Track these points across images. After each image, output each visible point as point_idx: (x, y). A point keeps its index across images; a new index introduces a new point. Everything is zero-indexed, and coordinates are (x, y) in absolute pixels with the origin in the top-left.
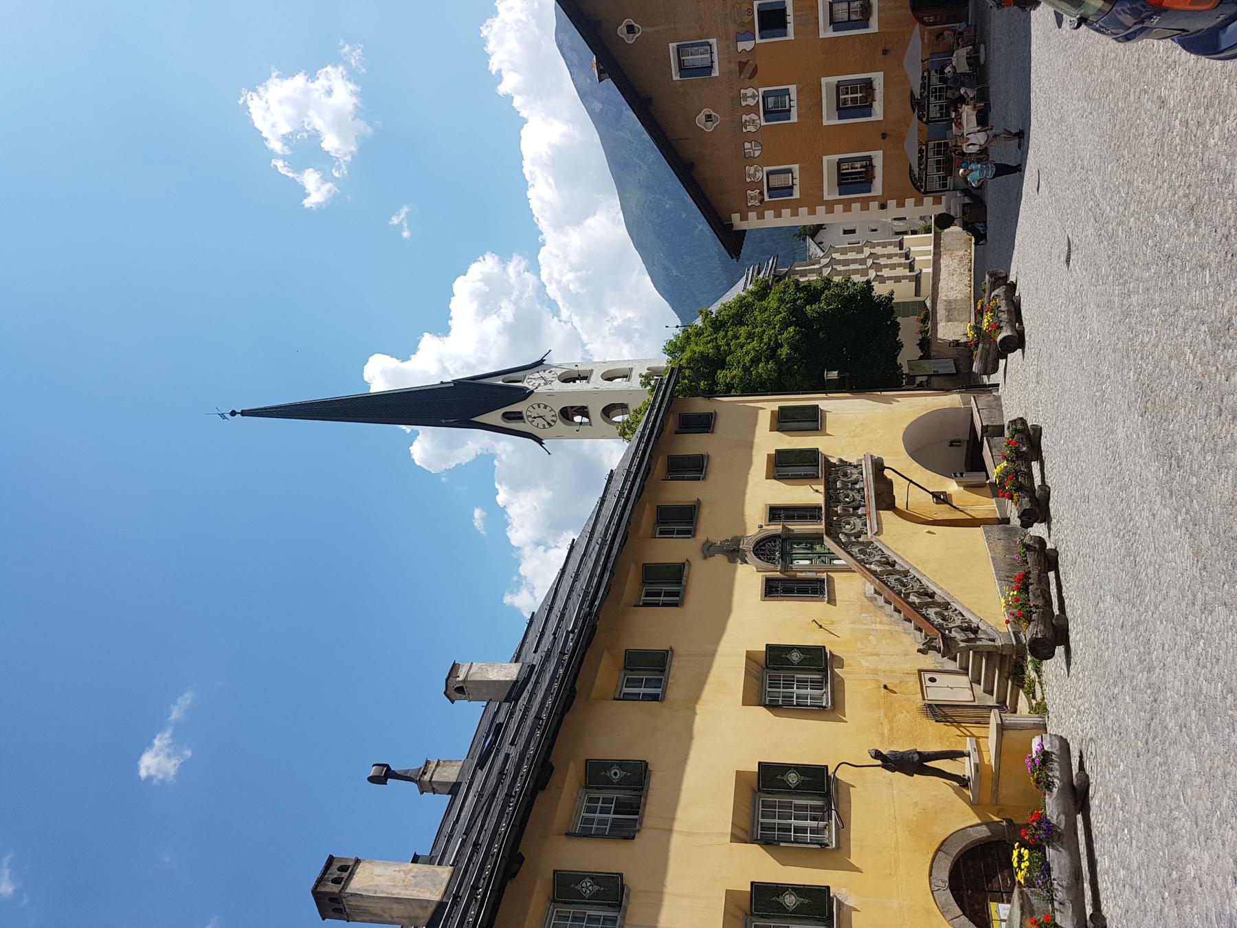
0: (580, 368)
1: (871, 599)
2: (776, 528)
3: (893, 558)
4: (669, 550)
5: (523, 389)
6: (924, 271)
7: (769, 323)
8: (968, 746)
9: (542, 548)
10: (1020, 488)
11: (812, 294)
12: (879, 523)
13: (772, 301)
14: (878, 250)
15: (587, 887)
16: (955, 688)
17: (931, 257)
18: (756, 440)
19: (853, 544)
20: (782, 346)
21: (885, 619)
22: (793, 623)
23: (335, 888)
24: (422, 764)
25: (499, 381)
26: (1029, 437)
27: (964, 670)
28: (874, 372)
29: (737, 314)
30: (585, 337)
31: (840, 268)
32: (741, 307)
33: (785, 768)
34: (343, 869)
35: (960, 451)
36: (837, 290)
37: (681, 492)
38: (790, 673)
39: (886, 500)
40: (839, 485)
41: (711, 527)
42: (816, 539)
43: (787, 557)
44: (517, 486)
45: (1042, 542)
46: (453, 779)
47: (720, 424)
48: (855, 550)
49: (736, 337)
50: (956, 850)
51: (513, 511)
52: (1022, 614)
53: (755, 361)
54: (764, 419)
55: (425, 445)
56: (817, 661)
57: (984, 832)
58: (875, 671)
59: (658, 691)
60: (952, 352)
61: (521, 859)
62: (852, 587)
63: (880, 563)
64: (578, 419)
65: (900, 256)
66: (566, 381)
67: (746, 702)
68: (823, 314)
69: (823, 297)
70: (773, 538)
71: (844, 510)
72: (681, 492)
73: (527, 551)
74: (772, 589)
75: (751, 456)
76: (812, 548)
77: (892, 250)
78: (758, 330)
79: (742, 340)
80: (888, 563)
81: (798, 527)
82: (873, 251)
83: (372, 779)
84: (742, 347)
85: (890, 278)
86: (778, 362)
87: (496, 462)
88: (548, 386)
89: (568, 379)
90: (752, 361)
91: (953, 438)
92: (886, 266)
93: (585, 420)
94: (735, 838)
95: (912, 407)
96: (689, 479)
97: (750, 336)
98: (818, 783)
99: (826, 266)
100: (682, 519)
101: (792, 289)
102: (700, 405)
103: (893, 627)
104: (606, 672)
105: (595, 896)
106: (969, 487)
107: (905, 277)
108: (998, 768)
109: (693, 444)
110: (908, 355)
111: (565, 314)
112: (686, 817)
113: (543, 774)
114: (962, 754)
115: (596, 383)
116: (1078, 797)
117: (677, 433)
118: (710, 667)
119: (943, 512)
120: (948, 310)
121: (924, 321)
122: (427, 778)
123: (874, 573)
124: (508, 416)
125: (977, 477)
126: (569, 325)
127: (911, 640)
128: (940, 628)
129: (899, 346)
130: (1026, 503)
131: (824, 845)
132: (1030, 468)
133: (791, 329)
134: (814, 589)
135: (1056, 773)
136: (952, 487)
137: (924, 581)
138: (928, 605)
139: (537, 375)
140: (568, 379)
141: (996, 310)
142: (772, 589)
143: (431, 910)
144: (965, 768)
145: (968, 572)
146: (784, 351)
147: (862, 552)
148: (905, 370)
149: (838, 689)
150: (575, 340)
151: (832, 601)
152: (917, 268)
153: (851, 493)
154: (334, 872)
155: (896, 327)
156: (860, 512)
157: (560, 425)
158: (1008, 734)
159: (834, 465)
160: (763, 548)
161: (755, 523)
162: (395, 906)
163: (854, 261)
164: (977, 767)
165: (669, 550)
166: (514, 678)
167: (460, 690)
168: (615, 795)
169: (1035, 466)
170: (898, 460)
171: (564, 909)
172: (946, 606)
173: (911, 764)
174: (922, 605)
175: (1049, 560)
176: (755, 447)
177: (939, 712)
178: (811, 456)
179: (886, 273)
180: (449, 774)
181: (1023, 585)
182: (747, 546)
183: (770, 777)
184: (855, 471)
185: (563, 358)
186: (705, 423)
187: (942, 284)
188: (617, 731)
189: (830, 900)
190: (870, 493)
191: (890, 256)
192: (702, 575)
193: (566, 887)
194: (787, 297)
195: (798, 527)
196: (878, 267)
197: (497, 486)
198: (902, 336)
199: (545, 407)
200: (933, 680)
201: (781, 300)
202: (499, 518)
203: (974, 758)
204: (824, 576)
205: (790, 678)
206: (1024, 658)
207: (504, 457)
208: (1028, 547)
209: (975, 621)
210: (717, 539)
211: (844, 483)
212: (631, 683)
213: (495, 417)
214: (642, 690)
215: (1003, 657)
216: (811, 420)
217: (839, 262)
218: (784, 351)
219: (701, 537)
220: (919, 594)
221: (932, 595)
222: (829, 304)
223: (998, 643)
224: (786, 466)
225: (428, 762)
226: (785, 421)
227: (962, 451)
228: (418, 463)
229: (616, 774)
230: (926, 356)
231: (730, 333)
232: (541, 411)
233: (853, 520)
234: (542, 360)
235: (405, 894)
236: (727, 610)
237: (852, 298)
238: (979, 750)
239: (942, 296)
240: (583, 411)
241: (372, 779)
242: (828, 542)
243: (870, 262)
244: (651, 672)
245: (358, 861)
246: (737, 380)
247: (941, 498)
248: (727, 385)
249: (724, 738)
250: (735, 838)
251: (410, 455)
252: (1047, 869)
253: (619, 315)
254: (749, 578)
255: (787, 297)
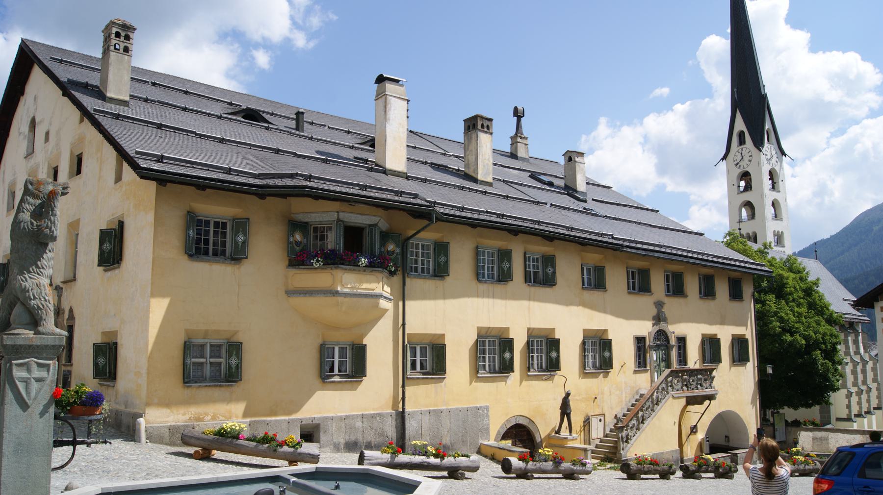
0: (781, 184)
1: (637, 392)
2: (673, 341)
3: (661, 404)
4: (658, 283)
5: (762, 144)
6: (855, 424)
7: (808, 327)
8: (574, 435)
9: (642, 140)
10: (700, 466)
11: (830, 354)
12: (678, 398)
13: (825, 328)
14: (874, 393)
15: (506, 265)
16: (597, 431)
17: (866, 429)
18: (726, 327)
19: (667, 384)
20: (792, 335)
21: (628, 399)
22: (623, 352)
23: (479, 127)
24: (525, 135)
25: (768, 126)
26: (727, 473)
27: (606, 436)
28: (770, 394)
29: (816, 304)
30: (816, 159)
31: (859, 368)
32: (821, 307)
33: (558, 351)
34: (488, 127)
35: (722, 441)
36: (832, 370)
37: (692, 285)
38: (496, 262)
39: (691, 401)
40: (700, 376)
41: (672, 305)
42: (668, 366)
43: (658, 347)
44: (691, 118)
45: (673, 473)
46: (519, 155)
47: (736, 304)
48: (664, 385)
49: (799, 305)
50: (531, 427)
51: (670, 117)
52: (640, 461)
53: (781, 319)
54: (739, 330)
55: (718, 45)
56: (606, 365)
57: (538, 440)
58: (603, 393)
59: (586, 285)
60: (791, 439)
61: (516, 235)
62: (644, 382)
63: (657, 398)
64: (743, 184)
65: (869, 408)
66: (771, 173)
67: (585, 331)
68: (814, 362)
69: (827, 361)
70: (667, 339)
71: (685, 380)
72: (692, 285)
73: (639, 129)
74: (640, 341)
75: (716, 324)
76: (663, 361)
77: (874, 403)
78: (804, 320)
79: (797, 309)
80: (658, 401)
81: (674, 354)
82: (854, 394)
83: (516, 109)
84: (791, 310)
85: (849, 402)
86: (780, 335)
87: (707, 100)
88: (765, 162)
89: (772, 175)
90: (781, 317)
91: (731, 439)
92: (860, 399)
93: (742, 189)
94: (529, 329)
95: (750, 417)
96: (700, 288)
97: (800, 315)
98: (553, 365)
99: (862, 358)
100: (676, 288)
101: (833, 340)
102: (748, 290)
103: (624, 403)
104: (594, 258)
105: (503, 269)
106: (700, 445)
107: (850, 411)
108: (567, 448)
109: (722, 289)
110: (789, 413)
111: (837, 142)
112: (535, 305)
113: (550, 237)
114: (570, 431)
115: (770, 196)
116: (570, 476)
117: (729, 278)
118: (599, 311)
119: (686, 431)
120: (821, 439)
121: (813, 423)
122: (519, 140)
123: (652, 395)
124: (741, 135)
125: (706, 448)
126: (825, 146)
127: (620, 410)
128: (627, 426)
129: (796, 408)
130: (692, 468)
131: (529, 370)
132: (711, 472)
133: (804, 342)
134: (641, 362)
135: (578, 468)
136: (700, 435)
137: (649, 419)
138: (638, 420)
139: (774, 152)
140: (772, 175)
141: (806, 463)
142: (640, 341)
143: (473, 175)
144: (564, 433)
145: (655, 439)
146: (788, 338)
147: (663, 389)
148: (781, 411)
149: (594, 375)
150: (811, 153)
151: (635, 372)
152: (858, 419)
153: (694, 383)
154: (486, 123)
155: (808, 406)
156: (685, 388)
157: (737, 172)
158: (583, 453)
159: (711, 373)
160: (662, 335)
161: (675, 329)
162: (474, 157)
163: (865, 377)
164: (566, 438)
165: (658, 283)
166: (578, 189)
167: (570, 159)
168: (540, 270)
169: (712, 475)
170: (715, 408)
171: (496, 256)
172: (638, 429)
173: (565, 409)
174: (638, 417)
175: (665, 475)
176: (721, 327)
177: (587, 422)
178: (716, 358)
179: (854, 399)
180: (521, 153)
181: (654, 462)
182: (662, 326)
183: (554, 344)
184: (708, 385)
185: (786, 170)
186: (736, 294)
187: (841, 435)
188: (568, 268)
189: (508, 373)
190: (695, 393)
191: (868, 401)
192: (645, 302)
193: (505, 255)
194: (827, 338)
195: (674, 354)
196: (860, 393)
197: (688, 103)
198: (802, 410)
199: (750, 161)
200: (600, 420)
201: (825, 334)
202: (664, 106)
203: (570, 437)
204: (648, 368)
205: (598, 352)
206: (615, 463)
207: (712, 105)
208: (671, 467)
209: (631, 442)
210: (665, 310)
211: (701, 379)
212: (589, 270)
213: (740, 125)
214: (585, 277)
215: (615, 453)
216: (740, 355)
217: (864, 366)
218: (788, 338)
219: (667, 300)
220: (643, 416)
221: (642, 422)
222: (822, 365)
223: (622, 452)
224: (711, 346)
225: (526, 138)
226: (739, 343)
227: (722, 442)
228: (704, 42)
229: (550, 270)
230: (787, 424)
231: (802, 301)
232: (746, 158)
233: (680, 384)
234: (785, 155)
235: (480, 161)
236: (627, 317)
237: (828, 380)
238: (574, 439)
239: (831, 435)
240: (748, 187)
241: (516, 109)
242: (667, 371)
243: (864, 388)
244: (596, 281)
245: (491, 134)
246: (767, 308)
247: (694, 430)
248: (765, 301)
249: (568, 320)
250: (529, 329)
251: (709, 35)
252: (546, 461)
253: (837, 186)
254: (645, 328)
255: (827, 338)
